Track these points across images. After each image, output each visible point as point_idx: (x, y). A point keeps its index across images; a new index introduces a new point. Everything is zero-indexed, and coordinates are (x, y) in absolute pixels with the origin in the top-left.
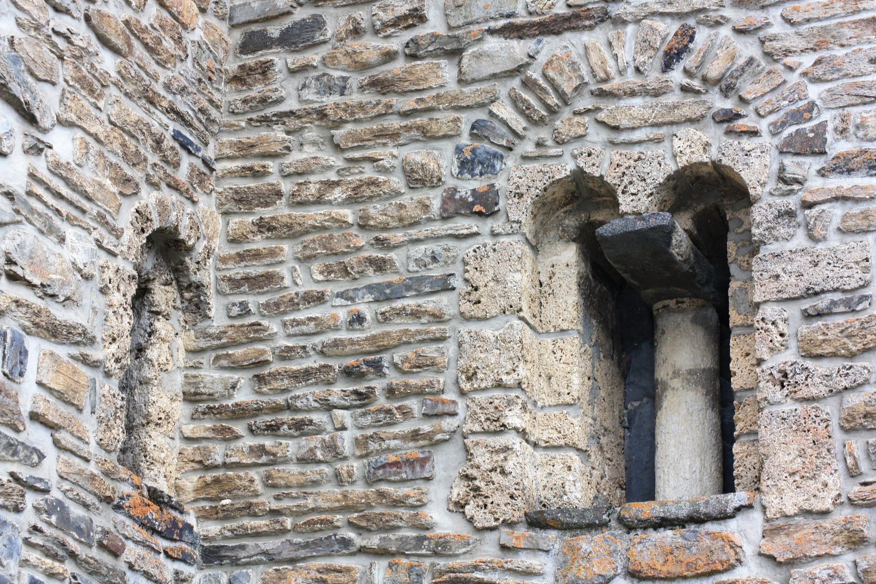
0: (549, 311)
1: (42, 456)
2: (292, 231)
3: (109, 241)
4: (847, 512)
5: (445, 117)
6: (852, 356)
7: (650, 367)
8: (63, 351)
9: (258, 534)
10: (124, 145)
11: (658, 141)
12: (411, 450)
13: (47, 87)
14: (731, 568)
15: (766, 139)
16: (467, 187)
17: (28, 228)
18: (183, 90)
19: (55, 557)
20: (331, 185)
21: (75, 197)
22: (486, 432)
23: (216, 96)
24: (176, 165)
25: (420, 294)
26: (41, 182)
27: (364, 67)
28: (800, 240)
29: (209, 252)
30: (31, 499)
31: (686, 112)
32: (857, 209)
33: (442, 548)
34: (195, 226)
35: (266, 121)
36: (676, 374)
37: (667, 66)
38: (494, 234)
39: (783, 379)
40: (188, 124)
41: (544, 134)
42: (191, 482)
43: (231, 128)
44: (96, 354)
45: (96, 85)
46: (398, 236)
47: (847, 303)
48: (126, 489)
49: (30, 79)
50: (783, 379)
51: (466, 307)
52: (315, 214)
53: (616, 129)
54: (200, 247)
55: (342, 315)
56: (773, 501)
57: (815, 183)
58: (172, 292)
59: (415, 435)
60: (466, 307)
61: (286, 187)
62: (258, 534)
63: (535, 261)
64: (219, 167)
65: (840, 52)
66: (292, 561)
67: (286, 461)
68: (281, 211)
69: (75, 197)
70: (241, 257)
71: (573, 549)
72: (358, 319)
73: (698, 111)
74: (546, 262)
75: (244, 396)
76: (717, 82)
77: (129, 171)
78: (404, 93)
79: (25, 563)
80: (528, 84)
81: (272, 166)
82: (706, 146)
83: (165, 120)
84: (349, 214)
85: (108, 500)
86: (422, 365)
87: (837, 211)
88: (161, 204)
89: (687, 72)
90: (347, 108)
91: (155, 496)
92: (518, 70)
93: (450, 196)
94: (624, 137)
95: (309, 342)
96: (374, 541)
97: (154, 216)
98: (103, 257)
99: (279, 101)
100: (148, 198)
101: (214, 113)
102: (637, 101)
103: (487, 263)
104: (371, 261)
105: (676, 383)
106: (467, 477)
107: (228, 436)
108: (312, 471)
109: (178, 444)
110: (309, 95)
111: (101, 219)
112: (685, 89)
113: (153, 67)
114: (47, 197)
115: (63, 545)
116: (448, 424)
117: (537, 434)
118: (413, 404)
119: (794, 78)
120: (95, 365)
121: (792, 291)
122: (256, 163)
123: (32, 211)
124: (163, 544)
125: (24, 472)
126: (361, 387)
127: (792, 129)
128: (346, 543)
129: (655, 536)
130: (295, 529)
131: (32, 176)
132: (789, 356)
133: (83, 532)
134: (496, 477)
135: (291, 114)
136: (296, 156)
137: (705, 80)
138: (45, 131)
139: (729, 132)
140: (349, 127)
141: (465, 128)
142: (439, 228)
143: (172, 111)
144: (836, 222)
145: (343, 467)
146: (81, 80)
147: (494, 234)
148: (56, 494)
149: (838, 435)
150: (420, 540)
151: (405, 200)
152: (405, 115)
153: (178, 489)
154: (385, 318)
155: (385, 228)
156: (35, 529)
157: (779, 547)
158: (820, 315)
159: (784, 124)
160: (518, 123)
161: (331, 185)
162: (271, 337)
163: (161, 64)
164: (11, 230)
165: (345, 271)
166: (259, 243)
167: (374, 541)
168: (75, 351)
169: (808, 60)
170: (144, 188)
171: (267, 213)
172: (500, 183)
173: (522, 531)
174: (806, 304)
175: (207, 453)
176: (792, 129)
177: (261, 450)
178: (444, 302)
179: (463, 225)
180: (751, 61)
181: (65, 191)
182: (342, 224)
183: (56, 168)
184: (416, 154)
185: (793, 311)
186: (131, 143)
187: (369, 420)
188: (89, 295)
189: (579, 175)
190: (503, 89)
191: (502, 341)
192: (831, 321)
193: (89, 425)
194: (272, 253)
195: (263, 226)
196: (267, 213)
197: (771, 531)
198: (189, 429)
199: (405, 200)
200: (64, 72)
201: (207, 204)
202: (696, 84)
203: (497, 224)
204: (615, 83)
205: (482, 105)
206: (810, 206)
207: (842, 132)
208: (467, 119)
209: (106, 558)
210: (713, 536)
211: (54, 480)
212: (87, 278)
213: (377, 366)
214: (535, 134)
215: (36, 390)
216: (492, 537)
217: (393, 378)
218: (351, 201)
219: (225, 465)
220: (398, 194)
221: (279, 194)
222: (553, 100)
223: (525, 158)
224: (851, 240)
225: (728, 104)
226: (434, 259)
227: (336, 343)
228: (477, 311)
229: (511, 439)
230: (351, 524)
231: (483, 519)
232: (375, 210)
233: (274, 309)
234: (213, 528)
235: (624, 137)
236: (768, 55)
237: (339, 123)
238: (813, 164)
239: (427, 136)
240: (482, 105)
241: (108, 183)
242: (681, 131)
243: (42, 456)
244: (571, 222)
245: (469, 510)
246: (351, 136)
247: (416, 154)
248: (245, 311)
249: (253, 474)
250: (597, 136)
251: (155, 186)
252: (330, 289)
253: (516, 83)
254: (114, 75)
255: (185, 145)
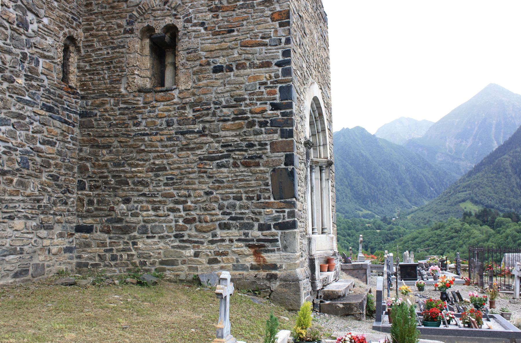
0: (144, 52)
1: (44, 81)
2: (96, 36)
3: (57, 39)
4: (193, 89)
5: (124, 14)
6: (195, 61)
7: (164, 62)
8: (47, 61)
9: (91, 94)
10: (60, 20)
11: (163, 19)
12: (118, 78)
13: (42, 10)
14: (173, 99)
15: (182, 20)
16: (128, 28)
17: (38, 38)
18: (73, 8)
19: (48, 99)
20: (103, 27)
21: (49, 31)
22: (131, 75)
23: (82, 9)
24: (73, 23)
25: (120, 48)
26: (41, 28)
27: (109, 4)
28: (187, 39)
29: (81, 40)
30: (42, 89)
31: (168, 14)
32: (197, 33)
33: (123, 96)
34: (77, 35)
35: (91, 14)
36: (168, 63)
37: (165, 5)
38: (133, 37)
39: (183, 65)
40: (75, 15)
41: (142, 18)
42: (78, 84)
43: (85, 16)
44: (55, 61)
45: (53, 9)
46: (116, 37)
47: (194, 51)
48: (63, 86)
49: (37, 8)
50: (183, 65)
51: (128, 51)
52: (100, 33)
53: (155, 17)
54: (79, 39)
55: (105, 52)
56: (180, 87)
57: (190, 28)
58: (74, 48)
59: (118, 75)
60: (128, 51)
61: (95, 27)
62: (91, 94)
63: (141, 42)
64: (82, 23)
65: (195, 3)
66: (97, 99)
67: (96, 80)
68: (94, 32)
69: (49, 31)
70: (87, 41)
71: (146, 96)
72: (108, 53)
73: (170, 14)
74: (144, 42)
75: (88, 68)
76: (174, 8)
77: (61, 25)
78: (117, 9)
79: (41, 100)
80: (140, 8)
81: (92, 23)
82: (171, 21)
83: (69, 14)
84: (107, 33)
85: (59, 88)
86: (120, 62)
87: (194, 34)
88: (69, 32)
89: (168, 6)
90: (106, 12)
91: (70, 87)
92: (138, 5)
93: (125, 30)
94: (156, 19)
95: (99, 58)
96: (111, 95)
97: (68, 34)
98: (56, 42)
99: (94, 10)
100: (66, 30)
101: (81, 12)
102: (159, 12)
103: (132, 43)
104: (111, 42)
105: (168, 65)
106: (128, 83)
107: (85, 75)
108: (100, 82)
109: (76, 77)
110: (99, 9)
111: (55, 35)
112: (168, 10)
113: (66, 4)
114: (42, 31)
115: (49, 97)
116: (124, 73)
117: (142, 75)
118: (118, 69)
119: (187, 8)
120: (55, 63)
121: (185, 49)
122: (89, 23)
123: (39, 34)
124: (72, 96)
125: (40, 84)
126: (109, 66)
127: (186, 18)
128: (106, 95)
129: (160, 94)
130: (97, 93)
131: (39, 27)
132: (184, 61)
133: (54, 94)
134: (133, 83)
135: (96, 13)
136: (97, 21)
137: (171, 8)
138: (41, 18)
139: (175, 18)
140: (107, 16)
141: (128, 16)
142: (123, 36)
143: (71, 13)
144: (193, 36)
145: (106, 81)
146: (49, 8)
147: (133, 37)
148: (47, 87)
149: (192, 75)
150: (119, 95)
151: (117, 30)
152: (117, 13)
153: (76, 85)
154: (113, 53)
155: (113, 36)
156: (43, 94)
157: (181, 96)
158: (190, 53)
159: (185, 17)
160: (137, 15)
161: (103, 27)
162: (93, 57)
163: (68, 3)
164: (35, 38)
165: (106, 44)
166: (90, 38)
167: (111, 95)
168: (50, 61)
169: (190, 4)
170: (65, 29)
171: (92, 32)
172: (134, 27)
173: (137, 93)
174: (187, 51)
175: (81, 79)
176: (186, 18)
177: (91, 78)
178: (123, 50)
179: (128, 35)
180: (179, 4)
181: (46, 30)
182: (105, 35)
183: (44, 26)
184: (119, 21)
185: (185, 52)
186: (62, 20)
187: (110, 72)
188: (53, 50)
189: (148, 26)
190: (135, 9)
191: (134, 58)
192: (192, 54)
193: (55, 75)
194: (93, 40)
195: (91, 35)
196: (92, 32)
197: (180, 93)
198: (78, 74)
199: (117, 30)
200: (45, 6)
201: (80, 31)
202: (170, 8)
203: (133, 35)
204: (155, 8)
205: (131, 12)
206: (189, 32)
207: (195, 18)
208: (128, 15)
209: (60, 99)
210: (170, 94)
211: (47, 85)
212: (53, 46)
213: (112, 62)
214: (140, 18)
215: (42, 68)
216: (132, 94)
217: (115, 65)
218: (107, 30)
219: (85, 81)
220: (115, 29)
221: (94, 29)
222: (144, 11)
223: (139, 22)
224: (196, 39)
225: (175, 13)
226: (122, 42)
227: (104, 58)
228: (129, 52)
229: (136, 77)
230: (107, 92)
231: (130, 91)
232: (111, 32)
233: (93, 51)
234: (83, 93)
235: (156, 19)
236: (183, 3)
237: (105, 15)
238: (190, 24)
239: (121, 18)
240: (131, 12)
241: (56, 28)
242: (167, 18)
243: (44, 81)
244: (148, 35)
245: (128, 89)
246: (107, 18)
247: (119, 21)
248: (88, 52)
249: (90, 83)
250: (152, 18)
251: (68, 28)
252: (103, 47)
253: (137, 8)
254: (57, 6)
255: (74, 19)
